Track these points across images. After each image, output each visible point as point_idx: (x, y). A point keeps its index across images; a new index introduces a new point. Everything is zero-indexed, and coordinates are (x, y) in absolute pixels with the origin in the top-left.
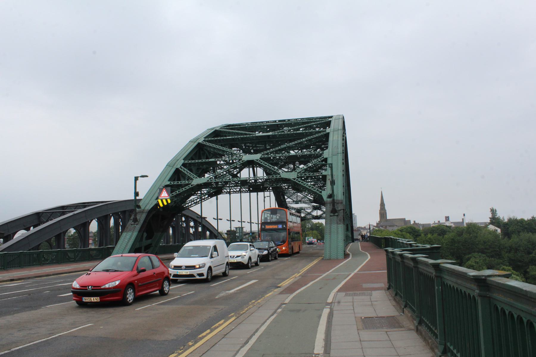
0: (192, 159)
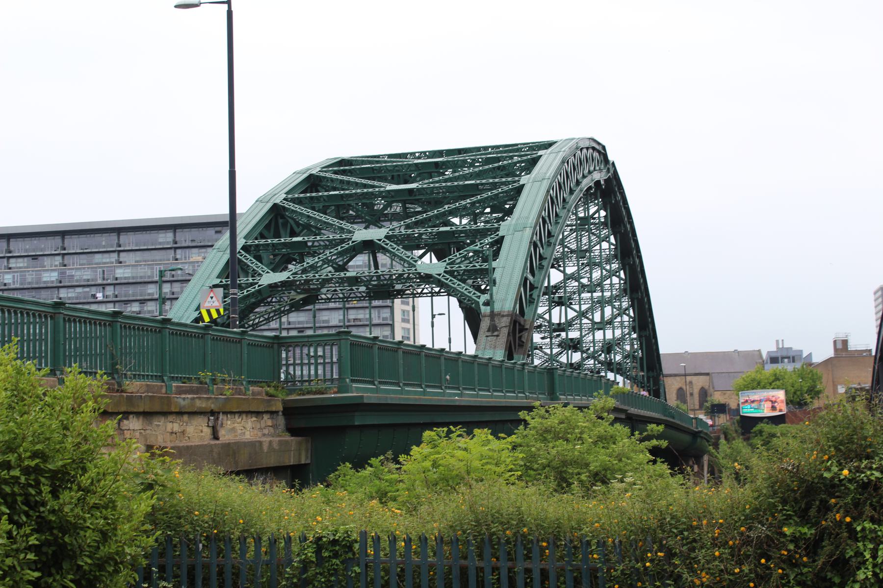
0: (262, 236)
